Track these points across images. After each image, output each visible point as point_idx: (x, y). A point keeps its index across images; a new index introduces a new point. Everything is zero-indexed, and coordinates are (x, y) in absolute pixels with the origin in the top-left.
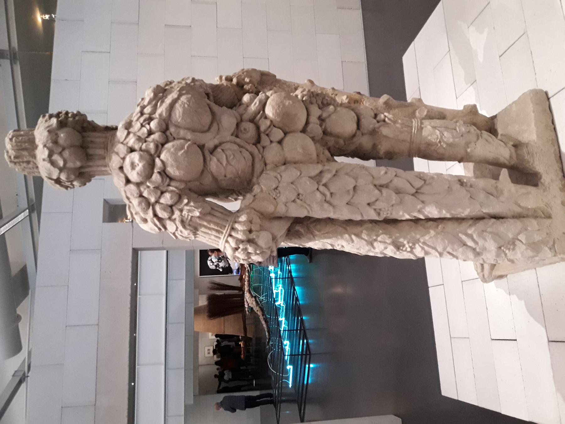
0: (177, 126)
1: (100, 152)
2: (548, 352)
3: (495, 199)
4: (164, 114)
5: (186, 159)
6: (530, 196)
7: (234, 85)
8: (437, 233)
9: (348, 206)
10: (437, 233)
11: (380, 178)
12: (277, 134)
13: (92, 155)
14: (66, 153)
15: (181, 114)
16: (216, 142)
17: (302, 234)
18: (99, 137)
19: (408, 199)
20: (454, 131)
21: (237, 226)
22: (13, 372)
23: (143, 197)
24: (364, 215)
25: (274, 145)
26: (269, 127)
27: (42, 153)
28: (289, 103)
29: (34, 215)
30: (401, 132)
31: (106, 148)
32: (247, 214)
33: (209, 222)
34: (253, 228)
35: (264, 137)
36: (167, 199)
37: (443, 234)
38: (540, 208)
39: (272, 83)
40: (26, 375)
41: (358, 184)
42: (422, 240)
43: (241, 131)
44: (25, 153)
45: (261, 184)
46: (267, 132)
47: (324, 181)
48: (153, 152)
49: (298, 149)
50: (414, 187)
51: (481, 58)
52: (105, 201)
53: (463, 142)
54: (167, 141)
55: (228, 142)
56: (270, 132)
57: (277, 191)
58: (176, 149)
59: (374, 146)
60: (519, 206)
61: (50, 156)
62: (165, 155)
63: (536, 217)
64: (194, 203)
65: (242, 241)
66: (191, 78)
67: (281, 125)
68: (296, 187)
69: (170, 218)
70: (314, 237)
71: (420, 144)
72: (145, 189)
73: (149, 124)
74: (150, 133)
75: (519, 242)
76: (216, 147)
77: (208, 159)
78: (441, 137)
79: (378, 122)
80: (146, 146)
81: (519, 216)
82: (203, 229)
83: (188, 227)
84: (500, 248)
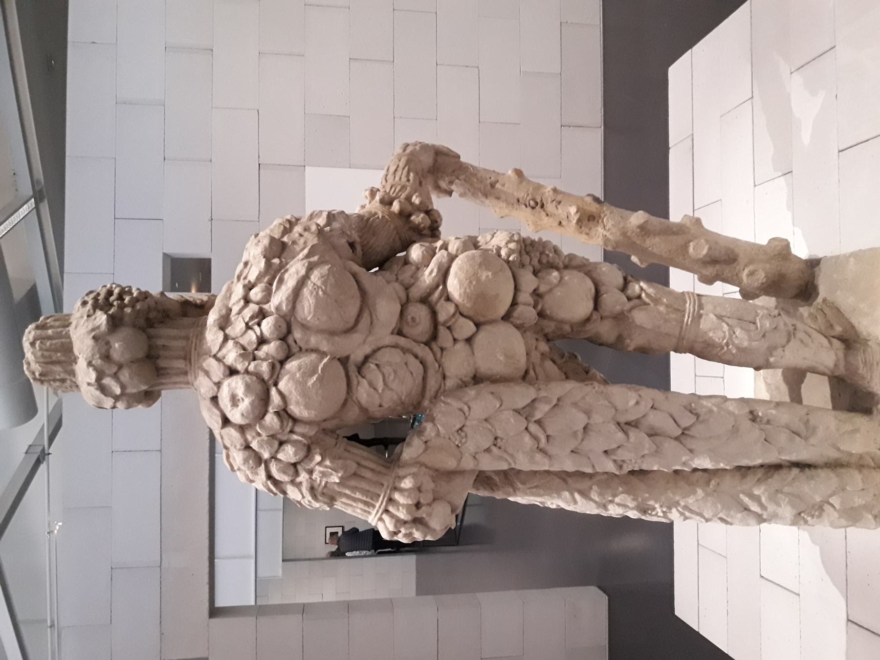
0: (305, 327)
1: (180, 364)
2: (845, 633)
3: (803, 441)
4: (284, 308)
5: (320, 392)
6: (858, 435)
7: (394, 213)
8: (707, 494)
9: (574, 454)
10: (707, 494)
11: (626, 410)
12: (466, 328)
13: (163, 369)
14: (125, 375)
15: (312, 310)
16: (368, 350)
17: (496, 485)
18: (175, 338)
19: (670, 446)
20: (752, 327)
21: (397, 496)
22: (27, 447)
23: (251, 448)
24: (596, 467)
25: (460, 346)
26: (454, 315)
27: (85, 374)
28: (487, 276)
29: (45, 208)
30: (666, 321)
31: (187, 358)
32: (414, 476)
33: (354, 489)
34: (422, 501)
35: (442, 330)
36: (288, 454)
37: (715, 494)
38: (867, 453)
39: (453, 171)
40: (46, 452)
41: (591, 422)
42: (682, 504)
43: (408, 323)
44: (58, 368)
45: (436, 422)
46: (448, 324)
47: (538, 416)
48: (266, 377)
49: (498, 355)
50: (679, 426)
51: (806, 137)
52: (165, 255)
53: (763, 345)
54: (289, 356)
55: (387, 346)
56: (454, 323)
57: (463, 434)
58: (304, 375)
59: (620, 338)
60: (839, 449)
61: (99, 379)
62: (286, 385)
63: (861, 467)
64: (331, 462)
65: (405, 522)
66: (325, 215)
67: (471, 314)
68: (493, 426)
69: (292, 482)
70: (515, 491)
71: (695, 341)
72: (254, 438)
73: (259, 325)
74: (262, 341)
75: (828, 506)
76: (367, 358)
77: (355, 382)
78: (731, 336)
79: (629, 299)
80: (255, 367)
81: (835, 465)
82: (344, 500)
83: (321, 498)
84: (800, 514)
